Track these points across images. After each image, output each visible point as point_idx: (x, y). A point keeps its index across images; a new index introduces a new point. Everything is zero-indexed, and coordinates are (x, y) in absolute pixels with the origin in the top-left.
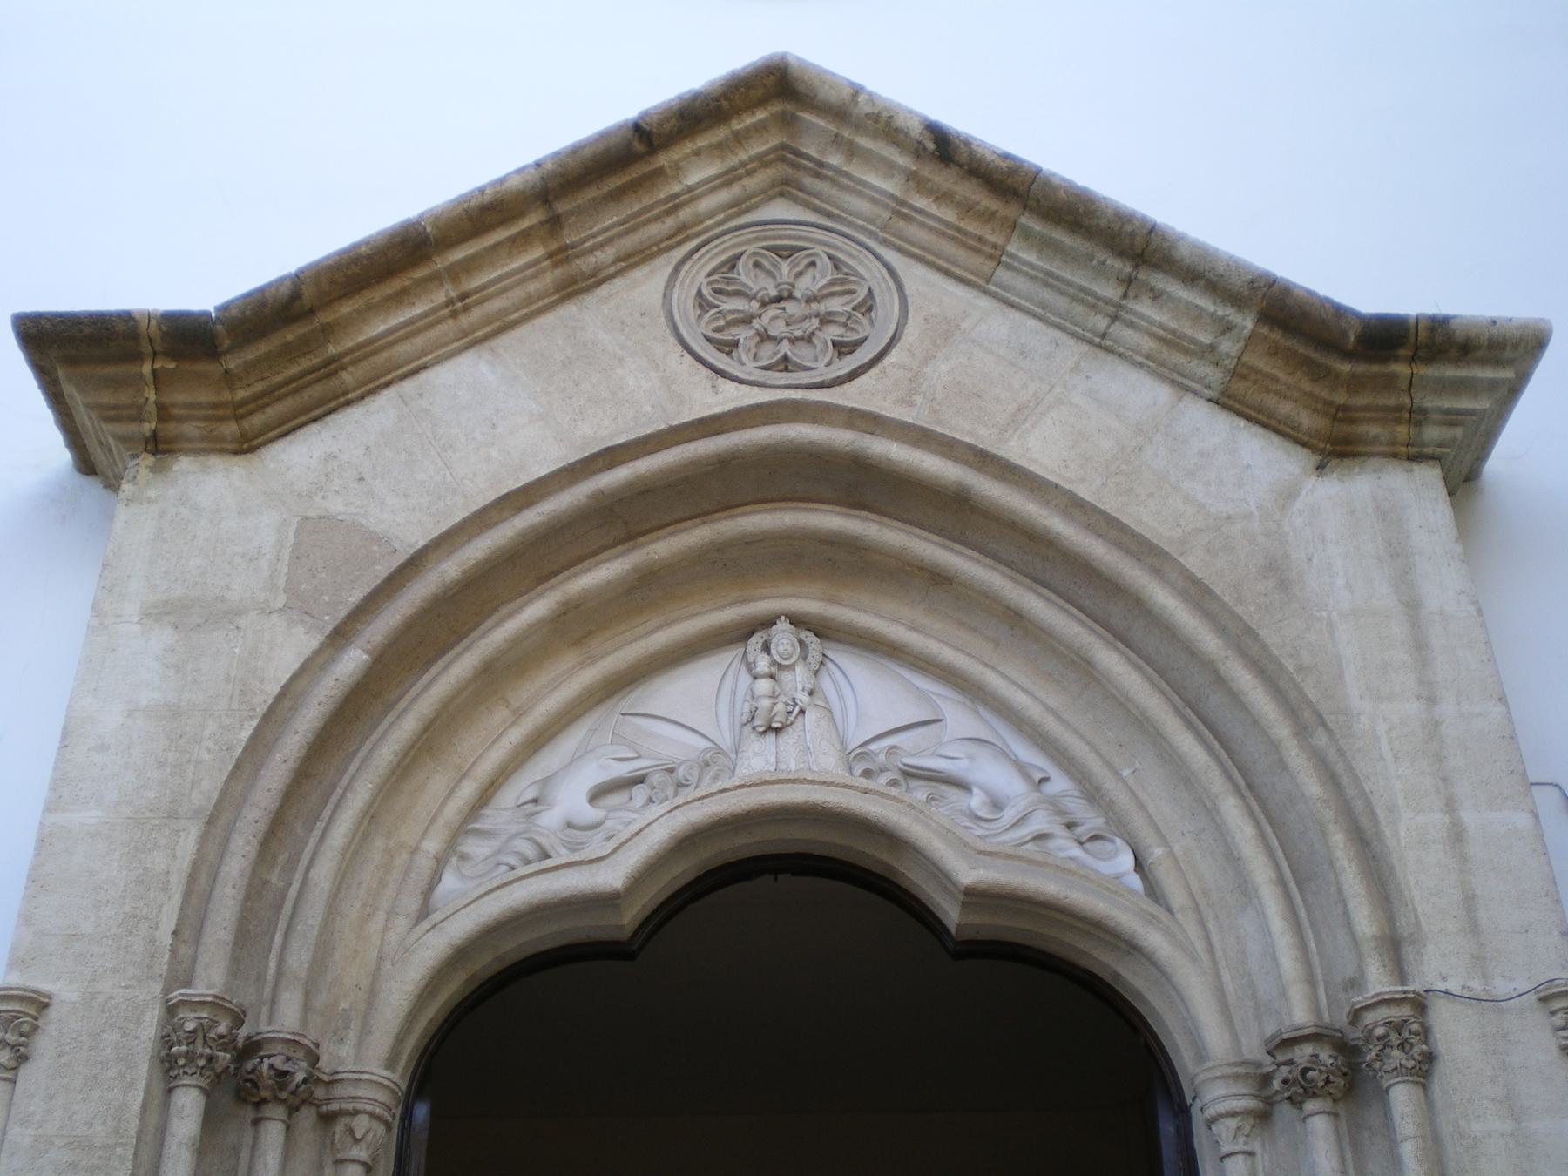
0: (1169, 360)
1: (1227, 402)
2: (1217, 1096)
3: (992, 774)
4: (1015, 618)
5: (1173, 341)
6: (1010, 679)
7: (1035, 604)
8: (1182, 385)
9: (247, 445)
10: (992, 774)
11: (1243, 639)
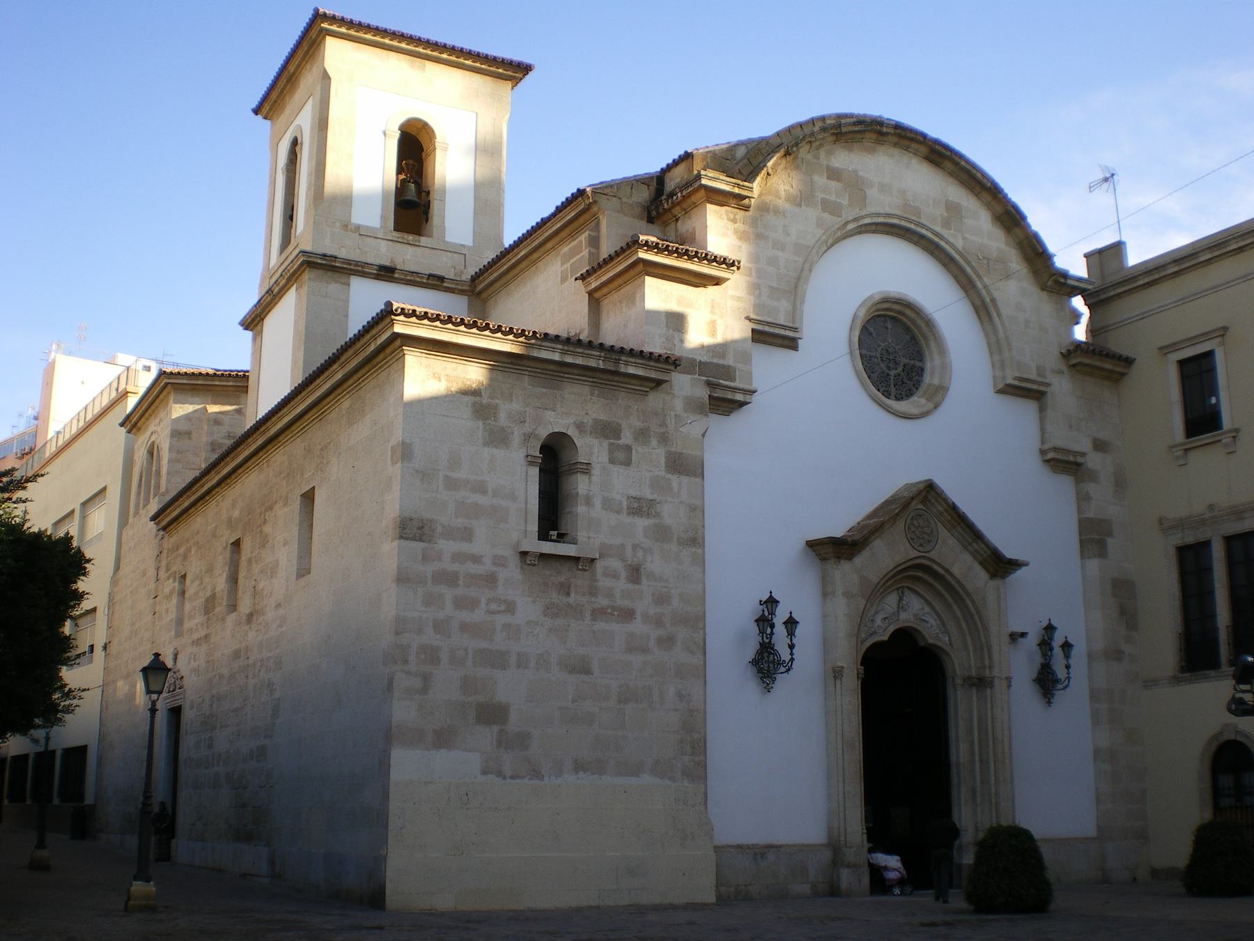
0: (974, 554)
1: (981, 563)
2: (958, 681)
3: (932, 622)
4: (931, 585)
5: (977, 551)
6: (938, 607)
7: (947, 595)
8: (975, 558)
9: (850, 559)
10: (932, 622)
11: (978, 612)
